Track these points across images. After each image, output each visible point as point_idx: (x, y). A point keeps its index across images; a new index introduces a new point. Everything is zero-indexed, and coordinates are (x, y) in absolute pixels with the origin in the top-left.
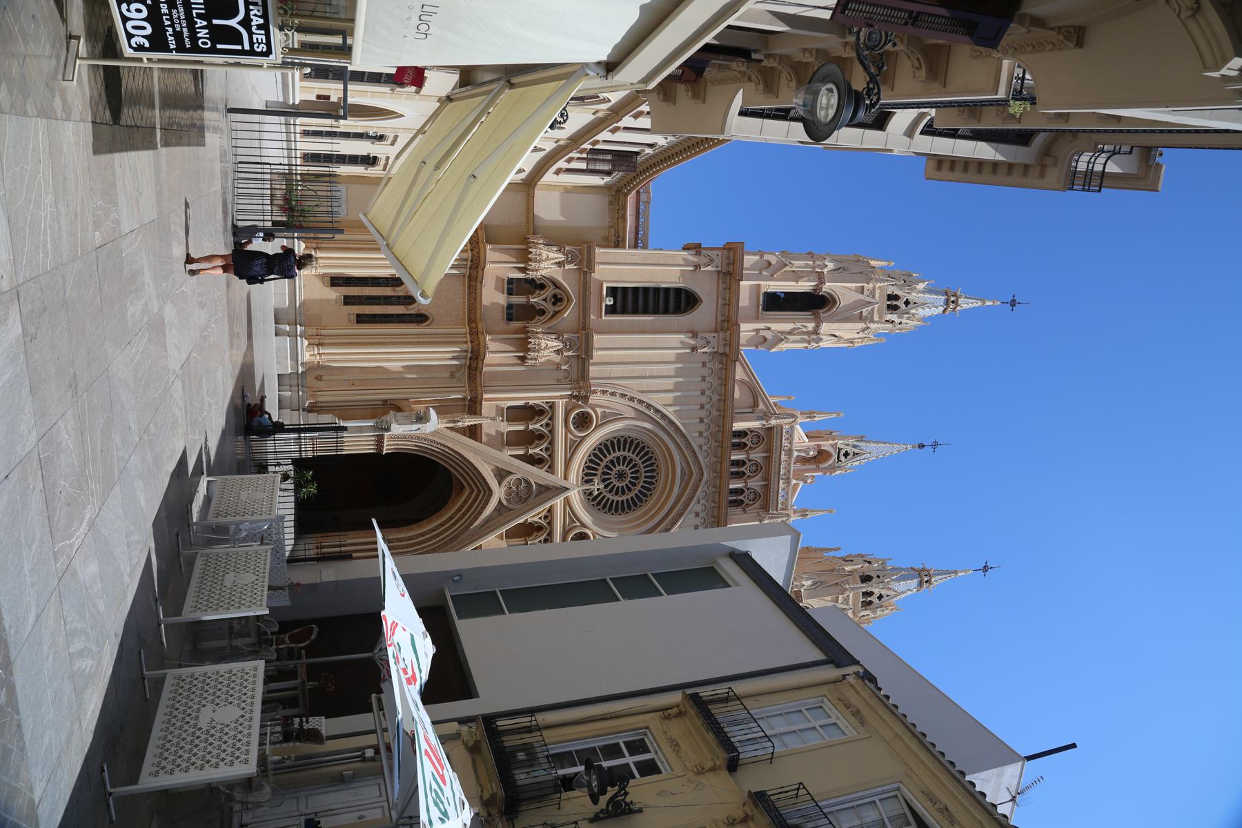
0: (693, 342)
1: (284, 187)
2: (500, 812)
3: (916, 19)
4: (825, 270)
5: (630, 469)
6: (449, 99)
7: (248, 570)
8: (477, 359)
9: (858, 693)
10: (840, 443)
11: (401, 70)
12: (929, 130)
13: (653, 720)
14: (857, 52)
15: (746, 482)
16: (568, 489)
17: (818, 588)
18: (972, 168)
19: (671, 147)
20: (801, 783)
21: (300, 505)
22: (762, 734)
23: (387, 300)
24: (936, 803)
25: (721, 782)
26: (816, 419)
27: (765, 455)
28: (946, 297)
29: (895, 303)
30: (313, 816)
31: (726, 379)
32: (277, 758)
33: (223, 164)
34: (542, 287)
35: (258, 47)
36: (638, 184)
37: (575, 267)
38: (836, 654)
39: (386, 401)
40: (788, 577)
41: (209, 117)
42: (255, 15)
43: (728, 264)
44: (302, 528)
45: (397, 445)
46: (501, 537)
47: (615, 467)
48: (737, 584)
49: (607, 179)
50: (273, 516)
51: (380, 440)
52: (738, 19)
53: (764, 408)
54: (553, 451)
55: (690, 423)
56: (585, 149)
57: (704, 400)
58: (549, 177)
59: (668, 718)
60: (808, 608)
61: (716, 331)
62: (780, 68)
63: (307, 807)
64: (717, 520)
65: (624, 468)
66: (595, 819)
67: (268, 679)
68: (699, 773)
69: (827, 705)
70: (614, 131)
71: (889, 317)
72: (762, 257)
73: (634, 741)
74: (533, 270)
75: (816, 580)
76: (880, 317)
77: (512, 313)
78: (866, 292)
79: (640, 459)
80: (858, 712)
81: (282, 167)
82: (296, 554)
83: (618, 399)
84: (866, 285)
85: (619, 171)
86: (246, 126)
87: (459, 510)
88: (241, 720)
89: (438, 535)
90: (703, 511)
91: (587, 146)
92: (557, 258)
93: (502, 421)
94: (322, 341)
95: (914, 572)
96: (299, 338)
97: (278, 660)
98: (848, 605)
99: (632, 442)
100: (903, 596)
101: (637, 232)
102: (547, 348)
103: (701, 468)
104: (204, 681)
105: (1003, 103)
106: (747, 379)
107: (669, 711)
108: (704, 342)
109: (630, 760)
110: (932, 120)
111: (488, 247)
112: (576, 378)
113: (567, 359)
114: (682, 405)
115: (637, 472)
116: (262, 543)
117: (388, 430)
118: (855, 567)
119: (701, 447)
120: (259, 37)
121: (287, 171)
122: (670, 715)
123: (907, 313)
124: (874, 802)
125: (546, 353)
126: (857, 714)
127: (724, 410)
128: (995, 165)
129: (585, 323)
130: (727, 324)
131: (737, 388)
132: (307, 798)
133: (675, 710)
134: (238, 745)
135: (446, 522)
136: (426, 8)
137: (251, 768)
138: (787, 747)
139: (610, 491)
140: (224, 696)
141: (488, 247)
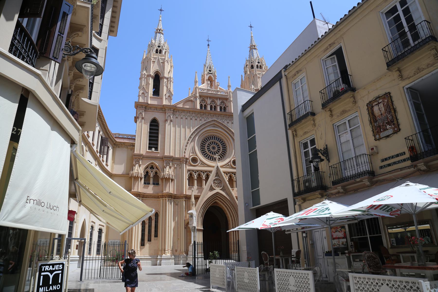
0: (169, 121)
1: (109, 262)
2: (325, 192)
3: (61, 33)
4: (146, 74)
5: (212, 145)
6: (80, 202)
7: (243, 274)
8: (171, 196)
9: (291, 71)
10: (206, 73)
11: (69, 218)
12: (100, 33)
13: (297, 140)
14: (71, 55)
15: (218, 106)
16: (217, 166)
17: (254, 83)
18: (114, 20)
19: (100, 125)
20: (320, 92)
21: (221, 258)
22: (303, 104)
23: (150, 226)
24: (328, 48)
25: (318, 118)
26: (197, 80)
27: (209, 98)
28: (158, 33)
29: (159, 51)
30: (324, 254)
31: (182, 110)
32: (305, 265)
33: (100, 282)
34: (147, 172)
35: (61, 268)
36: (113, 137)
37: (141, 161)
38: (278, 78)
39: (185, 228)
40: (251, 93)
41: (83, 287)
42: (49, 268)
43: (142, 107)
44: (228, 257)
45: (200, 224)
46: (233, 190)
47: (210, 150)
48: (253, 110)
49: (110, 148)
50: (225, 266)
51: (198, 230)
52: (57, 94)
53: (193, 98)
54: (204, 171)
55: (197, 123)
56: (99, 155)
57: (189, 118)
58: (109, 168)
59: (296, 135)
60: (261, 87)
61: (166, 113)
62: (75, 84)
63: (321, 256)
64: (231, 116)
65: (211, 147)
66: (329, 160)
67: (279, 267)
68: (315, 126)
69: (295, 82)
70: (93, 145)
71: (163, 53)
72: (140, 96)
73: (304, 147)
74: (141, 175)
75: (252, 84)
76: (163, 56)
77: (156, 183)
78: (155, 60)
79: (208, 141)
80: (297, 72)
81: (102, 262)
82: (237, 259)
83: (187, 148)
84: (152, 60)
85: (108, 144)
86: (87, 275)
87: (223, 204)
88: (294, 276)
89: (231, 211)
90: (227, 121)
91: (98, 154)
92: (138, 167)
93: (193, 188)
94: (163, 249)
95: (251, 51)
96: (162, 257)
97: (273, 265)
98: (261, 73)
99: (202, 144)
100: (259, 55)
101: (130, 139)
102: (169, 171)
103: (212, 121)
104: (280, 289)
105: (93, 6)
106: (182, 103)
107: (294, 135)
108: (169, 117)
109: (310, 148)
110: (96, 32)
111: (133, 191)
112: (179, 162)
113: (173, 165)
114: (190, 126)
115: (212, 142)
116: (234, 270)
117: (195, 227)
118: (248, 70)
119: (205, 120)
120: (57, 267)
121: (103, 261)
122: (295, 134)
123: (163, 47)
124: (327, 68)
125: (170, 172)
126: (298, 72)
127: (193, 112)
128: (113, 12)
129: (160, 158)
130: (163, 109)
131: (185, 107)
132: (319, 256)
133: (294, 132)
134: (302, 277)
135: (227, 208)
136: (48, 207)
137: (310, 273)
138: (307, 96)
139: (219, 152)
140: (286, 282)
141: (133, 191)
